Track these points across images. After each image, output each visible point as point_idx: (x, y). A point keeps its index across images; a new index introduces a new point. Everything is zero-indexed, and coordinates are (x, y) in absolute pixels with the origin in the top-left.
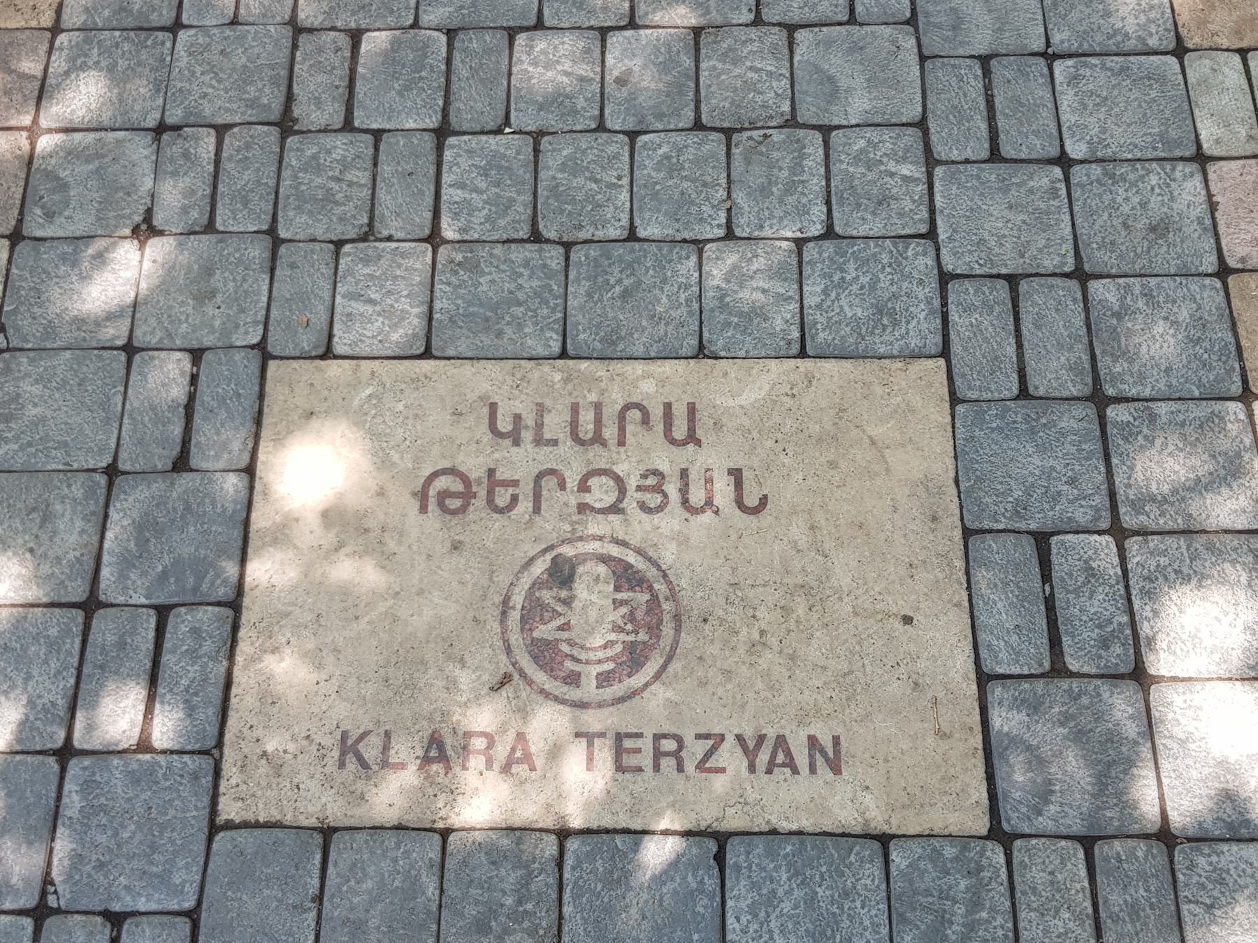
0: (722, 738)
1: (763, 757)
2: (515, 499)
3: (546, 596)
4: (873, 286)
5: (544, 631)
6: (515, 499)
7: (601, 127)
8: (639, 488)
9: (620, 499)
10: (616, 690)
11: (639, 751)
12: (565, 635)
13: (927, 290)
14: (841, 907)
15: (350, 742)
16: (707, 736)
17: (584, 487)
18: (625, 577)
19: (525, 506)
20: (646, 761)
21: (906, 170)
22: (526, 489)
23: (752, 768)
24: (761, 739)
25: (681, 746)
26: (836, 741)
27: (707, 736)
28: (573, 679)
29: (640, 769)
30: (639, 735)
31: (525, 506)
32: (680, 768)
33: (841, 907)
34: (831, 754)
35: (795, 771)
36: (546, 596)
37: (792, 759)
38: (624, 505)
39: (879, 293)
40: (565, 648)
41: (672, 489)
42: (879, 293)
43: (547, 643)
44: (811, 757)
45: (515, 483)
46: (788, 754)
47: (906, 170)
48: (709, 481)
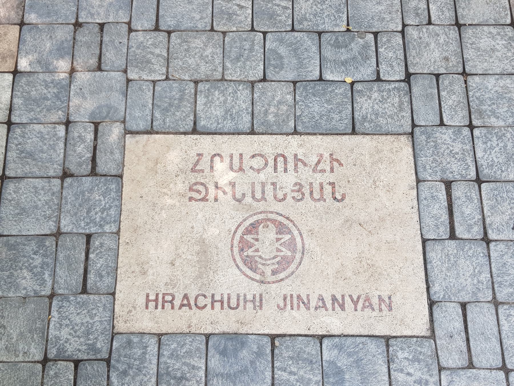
1: (360, 305)
4: (225, 102)
5: (250, 252)
7: (265, 33)
8: (293, 191)
12: (256, 254)
13: (246, 104)
18: (281, 229)
22: (271, 162)
25: (173, 299)
26: (308, 296)
32: (173, 308)
34: (341, 302)
35: (327, 310)
36: (249, 238)
37: (325, 305)
39: (227, 105)
40: (257, 259)
41: (306, 190)
42: (227, 105)
44: (333, 304)
48: (322, 188)
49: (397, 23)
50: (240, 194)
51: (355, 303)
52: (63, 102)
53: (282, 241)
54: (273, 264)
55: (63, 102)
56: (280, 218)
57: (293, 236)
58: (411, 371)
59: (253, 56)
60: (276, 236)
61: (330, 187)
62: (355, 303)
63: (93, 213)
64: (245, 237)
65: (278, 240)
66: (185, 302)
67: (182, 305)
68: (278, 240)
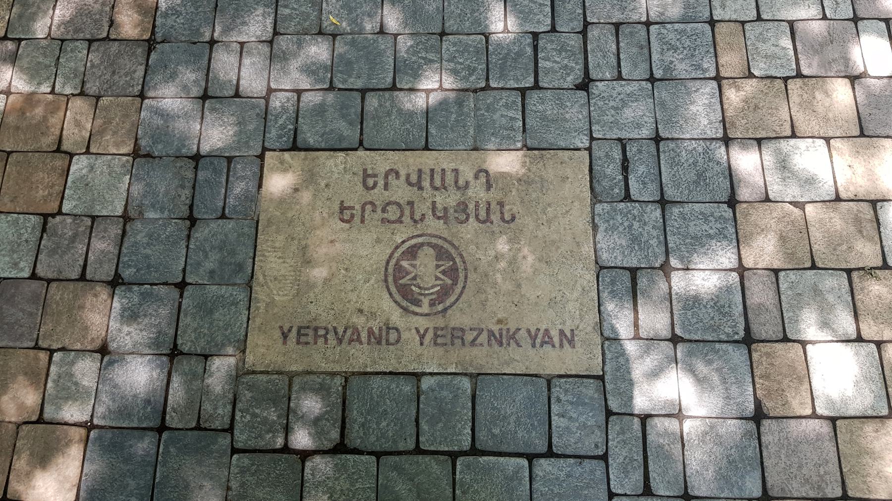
0: (483, 330)
1: (538, 341)
2: (352, 216)
3: (405, 264)
6: (352, 216)
9: (402, 215)
10: (440, 307)
11: (307, 335)
14: (366, 418)
15: (511, 333)
16: (474, 329)
17: (384, 210)
18: (441, 254)
19: (357, 219)
20: (310, 339)
21: (548, 64)
23: (534, 346)
24: (426, 330)
27: (474, 329)
28: (417, 303)
29: (307, 343)
30: (308, 327)
31: (357, 219)
33: (366, 418)
34: (498, 336)
35: (553, 346)
38: (403, 219)
40: (413, 288)
43: (405, 285)
44: (561, 341)
45: (352, 208)
46: (550, 338)
47: (548, 64)
49: (641, 13)
50: (419, 214)
51: (534, 338)
52: (595, 104)
53: (443, 268)
54: (432, 294)
55: (595, 104)
56: (434, 241)
57: (455, 263)
58: (574, 415)
59: (501, 59)
60: (435, 263)
61: (408, 207)
62: (534, 338)
63: (711, 232)
64: (451, 263)
65: (438, 266)
66: (546, 339)
67: (351, 341)
68: (438, 266)
